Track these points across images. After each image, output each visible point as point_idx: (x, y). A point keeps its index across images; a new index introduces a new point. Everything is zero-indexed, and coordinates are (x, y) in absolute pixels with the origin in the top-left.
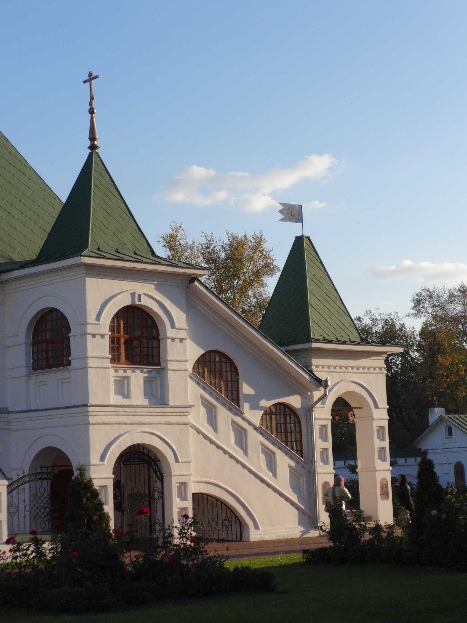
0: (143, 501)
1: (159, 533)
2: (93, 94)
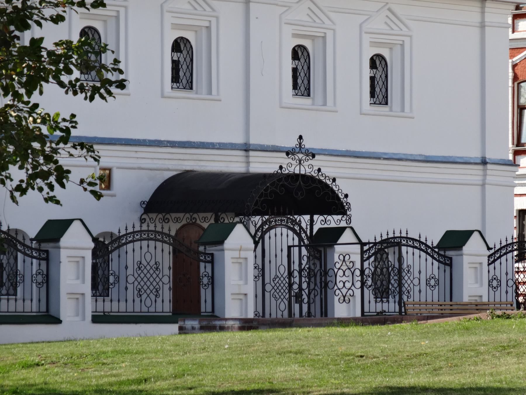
0: (273, 290)
2: (142, 245)
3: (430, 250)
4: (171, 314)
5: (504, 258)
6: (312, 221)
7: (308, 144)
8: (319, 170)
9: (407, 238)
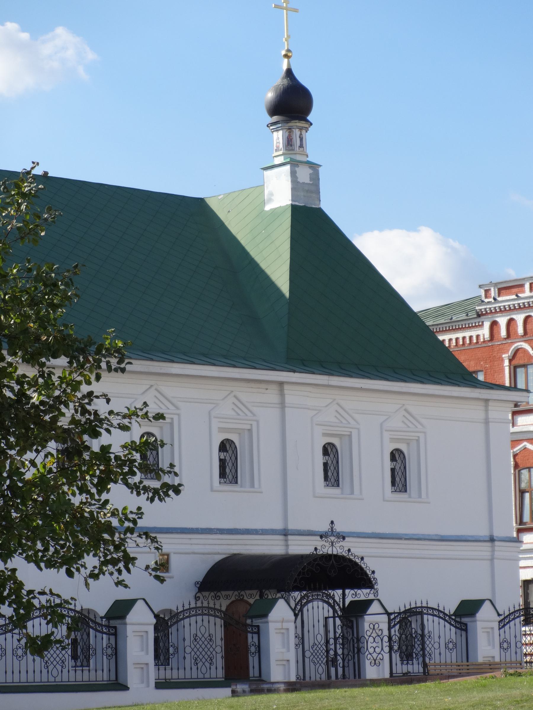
0: (312, 657)
1: (197, 596)
3: (448, 617)
4: (223, 679)
5: (512, 623)
6: (344, 594)
7: (338, 528)
8: (349, 550)
9: (427, 607)
